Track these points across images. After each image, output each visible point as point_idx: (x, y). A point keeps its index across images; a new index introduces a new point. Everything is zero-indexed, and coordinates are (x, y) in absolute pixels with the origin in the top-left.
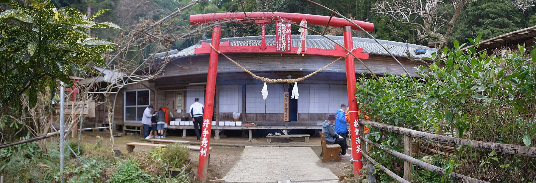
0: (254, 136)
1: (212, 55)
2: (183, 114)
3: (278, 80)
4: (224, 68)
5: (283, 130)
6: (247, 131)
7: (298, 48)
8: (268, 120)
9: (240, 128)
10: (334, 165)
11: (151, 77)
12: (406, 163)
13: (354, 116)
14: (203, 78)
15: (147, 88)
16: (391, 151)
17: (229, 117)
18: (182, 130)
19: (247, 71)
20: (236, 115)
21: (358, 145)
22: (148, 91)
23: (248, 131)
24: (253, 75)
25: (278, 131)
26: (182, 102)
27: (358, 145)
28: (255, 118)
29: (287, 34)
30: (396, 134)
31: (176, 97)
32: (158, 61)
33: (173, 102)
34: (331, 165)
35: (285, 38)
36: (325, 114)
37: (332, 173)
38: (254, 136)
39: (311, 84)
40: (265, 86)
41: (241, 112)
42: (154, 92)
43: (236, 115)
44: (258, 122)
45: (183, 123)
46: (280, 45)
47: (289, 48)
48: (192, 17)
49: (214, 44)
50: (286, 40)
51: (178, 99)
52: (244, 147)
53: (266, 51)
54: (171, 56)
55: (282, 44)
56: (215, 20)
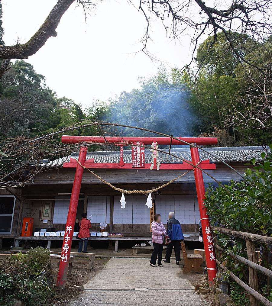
0: (120, 248)
1: (78, 169)
2: (49, 224)
3: (134, 191)
4: (87, 180)
5: (149, 241)
6: (114, 242)
7: (150, 164)
8: (135, 231)
9: (106, 239)
10: (195, 276)
11: (20, 184)
12: (249, 268)
13: (205, 223)
14: (69, 188)
15: (13, 194)
16: (237, 256)
17: (97, 228)
18: (47, 241)
19: (106, 183)
20: (103, 226)
21: (211, 252)
22: (13, 198)
23: (114, 242)
24: (113, 187)
25: (143, 242)
26: (49, 212)
27: (211, 252)
28: (122, 229)
29: (141, 154)
30: (242, 240)
31: (43, 206)
32: (29, 170)
33: (40, 211)
34: (191, 277)
35: (139, 157)
36: (192, 225)
37: (190, 284)
38: (120, 248)
39: (175, 194)
40: (123, 196)
41: (108, 222)
42: (20, 200)
43: (103, 226)
44: (124, 232)
45: (48, 234)
46: (135, 162)
47: (143, 164)
48: (64, 137)
49: (80, 160)
50: (141, 158)
51: (45, 209)
52: (109, 258)
53: (123, 168)
54: (42, 165)
55: (137, 161)
56: (81, 142)
